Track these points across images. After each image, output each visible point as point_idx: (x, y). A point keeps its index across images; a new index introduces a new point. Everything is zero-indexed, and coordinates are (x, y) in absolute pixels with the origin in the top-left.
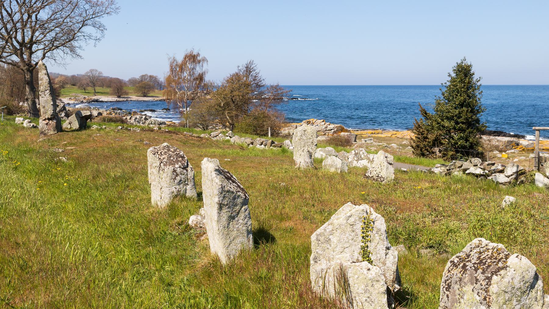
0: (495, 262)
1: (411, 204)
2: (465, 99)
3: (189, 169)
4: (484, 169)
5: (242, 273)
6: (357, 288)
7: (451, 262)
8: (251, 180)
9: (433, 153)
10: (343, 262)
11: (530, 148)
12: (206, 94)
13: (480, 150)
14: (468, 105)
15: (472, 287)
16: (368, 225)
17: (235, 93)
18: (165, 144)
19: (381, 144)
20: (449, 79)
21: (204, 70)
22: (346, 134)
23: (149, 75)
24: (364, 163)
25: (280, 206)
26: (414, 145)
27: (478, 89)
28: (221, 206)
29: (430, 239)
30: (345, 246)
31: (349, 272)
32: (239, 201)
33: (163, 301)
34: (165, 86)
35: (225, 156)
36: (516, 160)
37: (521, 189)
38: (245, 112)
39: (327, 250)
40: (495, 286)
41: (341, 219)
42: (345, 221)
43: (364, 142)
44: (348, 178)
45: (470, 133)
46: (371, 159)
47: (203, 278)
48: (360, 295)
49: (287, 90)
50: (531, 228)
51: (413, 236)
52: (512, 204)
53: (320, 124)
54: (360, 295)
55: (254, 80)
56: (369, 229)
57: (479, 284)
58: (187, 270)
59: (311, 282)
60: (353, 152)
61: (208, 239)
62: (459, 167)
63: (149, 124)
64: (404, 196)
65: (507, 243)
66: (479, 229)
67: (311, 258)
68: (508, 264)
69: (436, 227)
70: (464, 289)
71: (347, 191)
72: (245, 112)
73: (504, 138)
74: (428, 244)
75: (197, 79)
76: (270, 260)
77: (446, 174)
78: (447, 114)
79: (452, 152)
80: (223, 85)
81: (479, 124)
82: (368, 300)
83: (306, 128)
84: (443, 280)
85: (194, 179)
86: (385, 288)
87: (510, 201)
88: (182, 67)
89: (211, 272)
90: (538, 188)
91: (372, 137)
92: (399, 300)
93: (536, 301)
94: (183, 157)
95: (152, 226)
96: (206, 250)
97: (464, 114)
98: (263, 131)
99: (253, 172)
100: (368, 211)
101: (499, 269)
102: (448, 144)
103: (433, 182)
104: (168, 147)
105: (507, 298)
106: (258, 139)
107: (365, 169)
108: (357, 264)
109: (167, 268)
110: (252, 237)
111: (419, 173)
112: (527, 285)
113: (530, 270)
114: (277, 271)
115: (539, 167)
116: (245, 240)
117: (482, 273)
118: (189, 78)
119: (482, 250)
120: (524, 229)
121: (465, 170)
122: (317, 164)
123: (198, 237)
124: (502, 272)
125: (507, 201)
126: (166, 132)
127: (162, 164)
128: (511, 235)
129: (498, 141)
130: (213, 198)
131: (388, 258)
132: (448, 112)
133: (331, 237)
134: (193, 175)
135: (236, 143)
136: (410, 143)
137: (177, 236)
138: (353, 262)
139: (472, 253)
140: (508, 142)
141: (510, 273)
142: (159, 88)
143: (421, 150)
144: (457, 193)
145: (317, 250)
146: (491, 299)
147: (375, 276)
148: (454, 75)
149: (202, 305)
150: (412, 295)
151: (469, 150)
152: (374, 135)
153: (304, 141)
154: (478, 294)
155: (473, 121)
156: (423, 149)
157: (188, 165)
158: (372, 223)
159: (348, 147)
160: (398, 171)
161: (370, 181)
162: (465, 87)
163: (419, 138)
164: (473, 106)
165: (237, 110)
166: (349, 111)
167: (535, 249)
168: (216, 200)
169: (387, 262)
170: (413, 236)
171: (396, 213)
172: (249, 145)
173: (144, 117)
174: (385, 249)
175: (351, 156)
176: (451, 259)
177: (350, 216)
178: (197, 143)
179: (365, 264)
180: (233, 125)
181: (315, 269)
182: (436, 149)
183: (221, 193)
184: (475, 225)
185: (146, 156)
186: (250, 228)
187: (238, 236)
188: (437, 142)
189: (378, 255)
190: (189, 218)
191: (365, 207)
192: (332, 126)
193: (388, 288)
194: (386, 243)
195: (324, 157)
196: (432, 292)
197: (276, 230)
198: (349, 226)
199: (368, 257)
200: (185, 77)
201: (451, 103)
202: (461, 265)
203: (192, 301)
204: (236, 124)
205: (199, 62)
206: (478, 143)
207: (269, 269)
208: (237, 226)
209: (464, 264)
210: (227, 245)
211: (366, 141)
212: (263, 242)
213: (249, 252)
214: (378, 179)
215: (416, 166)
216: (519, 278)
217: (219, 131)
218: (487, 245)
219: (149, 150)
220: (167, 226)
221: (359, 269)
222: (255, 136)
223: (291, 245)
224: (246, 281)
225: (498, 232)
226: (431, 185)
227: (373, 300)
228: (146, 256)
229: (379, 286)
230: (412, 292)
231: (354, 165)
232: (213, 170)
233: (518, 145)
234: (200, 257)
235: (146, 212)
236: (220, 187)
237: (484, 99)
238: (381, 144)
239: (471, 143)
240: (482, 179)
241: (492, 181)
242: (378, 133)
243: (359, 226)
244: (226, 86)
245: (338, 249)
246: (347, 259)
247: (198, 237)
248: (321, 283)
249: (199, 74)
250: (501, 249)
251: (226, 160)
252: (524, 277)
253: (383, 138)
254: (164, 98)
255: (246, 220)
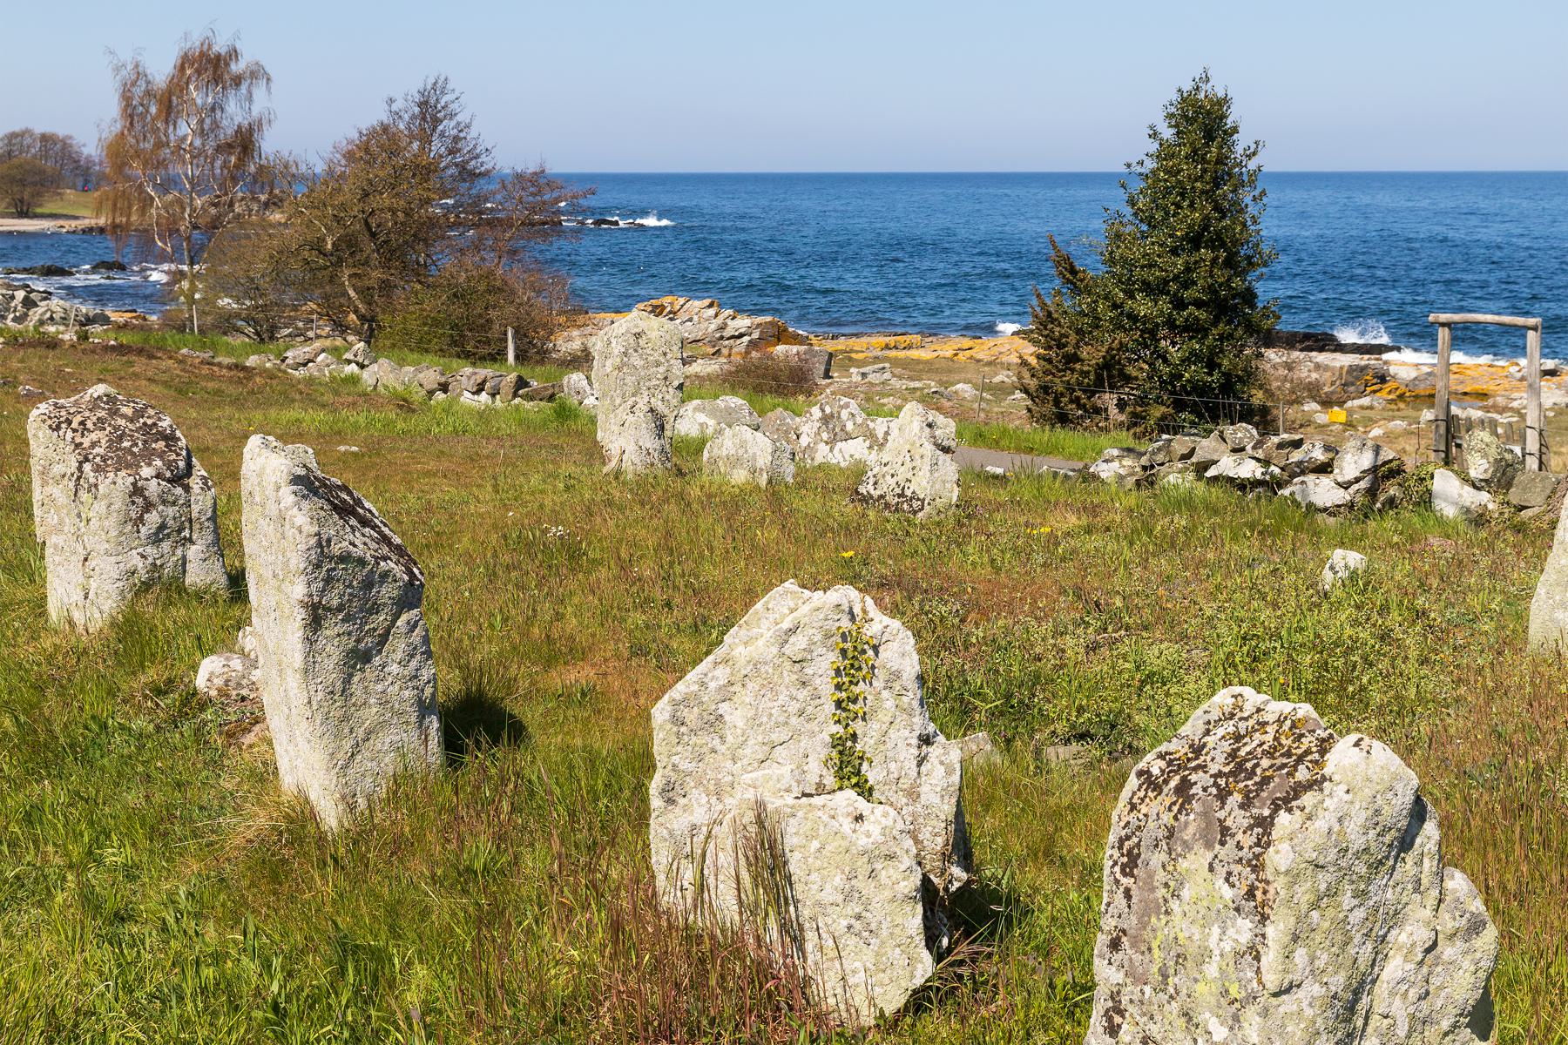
0: (1284, 766)
1: (1014, 589)
2: (1206, 218)
3: (195, 483)
4: (1266, 462)
5: (401, 861)
6: (816, 884)
7: (1140, 774)
8: (437, 521)
9: (1097, 411)
10: (767, 797)
11: (1422, 389)
12: (266, 205)
13: (1258, 397)
14: (1217, 242)
15: (1209, 856)
16: (855, 658)
17: (376, 202)
18: (100, 389)
19: (917, 384)
20: (1154, 147)
21: (255, 113)
22: (795, 349)
23: (39, 129)
24: (853, 450)
25: (546, 610)
26: (1033, 384)
27: (1252, 182)
28: (316, 616)
29: (1081, 710)
30: (776, 737)
31: (791, 830)
32: (387, 592)
33: (92, 977)
34: (102, 177)
35: (340, 436)
36: (1376, 432)
37: (1385, 527)
38: (419, 272)
39: (709, 758)
40: (1284, 847)
41: (760, 643)
42: (774, 650)
43: (856, 378)
44: (797, 503)
45: (1221, 338)
46: (880, 436)
47: (253, 884)
48: (830, 910)
49: (577, 189)
50: (1413, 654)
51: (1021, 702)
52: (1353, 576)
53: (700, 316)
54: (830, 910)
55: (451, 152)
56: (861, 674)
57: (1231, 843)
58: (191, 861)
59: (653, 877)
60: (816, 412)
61: (270, 743)
62: (1184, 457)
63: (42, 323)
64: (993, 561)
65: (1336, 709)
66: (1249, 662)
67: (655, 785)
68: (1327, 771)
69: (1098, 667)
70: (1183, 864)
71: (789, 549)
72: (419, 272)
73: (1337, 355)
74: (1073, 727)
75: (230, 146)
76: (506, 806)
77: (1138, 483)
78: (1145, 274)
79: (1163, 409)
80: (330, 172)
81: (1253, 306)
82: (858, 925)
83: (643, 325)
84: (1112, 838)
85: (213, 519)
86: (916, 879)
87: (1346, 567)
88: (169, 102)
89: (284, 861)
90: (1441, 521)
91: (886, 359)
92: (966, 922)
93: (1416, 890)
94: (170, 439)
95: (51, 701)
96: (262, 780)
97: (1203, 271)
98: (488, 343)
99: (447, 491)
100: (857, 610)
101: (1299, 789)
102: (1150, 378)
103: (1094, 510)
104: (111, 399)
105: (1323, 887)
106: (468, 370)
107: (859, 472)
108: (817, 800)
109: (113, 855)
110: (436, 725)
111: (1048, 481)
112: (1388, 839)
113: (1399, 787)
114: (532, 845)
115: (1447, 452)
116: (411, 737)
117: (1242, 806)
118: (198, 143)
119: (1242, 726)
120: (1394, 659)
121: (1202, 468)
122: (682, 456)
123: (230, 735)
124: (1308, 799)
125: (1340, 566)
126: (107, 349)
127: (87, 467)
128: (1351, 682)
129: (1318, 366)
130: (287, 587)
131: (927, 772)
132: (1150, 266)
133: (724, 708)
134: (210, 503)
135: (381, 389)
136: (1020, 378)
137: (149, 737)
138: (805, 795)
139: (1210, 740)
140: (1351, 369)
141: (1334, 799)
142: (80, 182)
143: (1057, 403)
144: (1173, 545)
145: (675, 759)
146: (1270, 895)
147: (881, 839)
148: (1168, 133)
149: (248, 983)
150: (1011, 899)
151: (1220, 400)
152: (893, 353)
153: (635, 375)
154: (1227, 880)
155: (1234, 297)
156: (1063, 397)
157: (189, 466)
158: (870, 653)
159: (801, 398)
160: (972, 477)
161: (872, 514)
162: (1208, 177)
163: (1050, 361)
164: (1235, 242)
165: (386, 265)
166: (802, 267)
167: (1424, 728)
168: (299, 590)
169: (924, 789)
170: (1021, 702)
171: (962, 621)
172: (431, 393)
173: (20, 295)
174: (915, 742)
175: (808, 427)
176: (1142, 765)
177: (792, 631)
178: (232, 390)
179: (848, 798)
180: (373, 319)
181: (668, 826)
182: (1109, 400)
183: (318, 566)
184: (1231, 654)
185: (26, 443)
186: (428, 691)
187: (382, 725)
188: (1110, 373)
189: (893, 766)
190: (195, 668)
191: (845, 594)
192: (743, 323)
193: (926, 880)
194: (921, 723)
195: (710, 431)
196: (1079, 888)
197: (528, 697)
198: (787, 664)
199: (858, 773)
200: (184, 139)
201: (1161, 234)
202: (1173, 784)
203: (209, 972)
204: (384, 319)
205: (237, 81)
206: (1249, 375)
207: (500, 838)
208: (379, 687)
209: (1184, 780)
210: (342, 757)
211: (864, 375)
212: (478, 744)
213: (424, 780)
214: (904, 504)
215: (1037, 460)
216: (1364, 814)
217: (318, 344)
218: (1259, 710)
219: (35, 412)
220: (109, 700)
221: (825, 818)
222: (455, 363)
223: (585, 747)
224: (416, 888)
225: (1309, 675)
226: (1084, 521)
227: (873, 926)
228: (28, 814)
229: (895, 875)
230: (1011, 889)
231: (819, 459)
232: (284, 478)
233: (1382, 379)
234: (237, 809)
235: (27, 652)
236: (313, 541)
237: (1270, 224)
238: (917, 384)
239: (1227, 375)
240: (1259, 498)
241: (1294, 501)
242: (910, 347)
243: (825, 663)
244: (342, 176)
245: (751, 751)
246: (783, 785)
247: (230, 735)
248: (688, 875)
249: (239, 131)
250: (1306, 720)
251: (342, 448)
252: (1377, 812)
253: (927, 362)
254: (102, 221)
255: (414, 663)
